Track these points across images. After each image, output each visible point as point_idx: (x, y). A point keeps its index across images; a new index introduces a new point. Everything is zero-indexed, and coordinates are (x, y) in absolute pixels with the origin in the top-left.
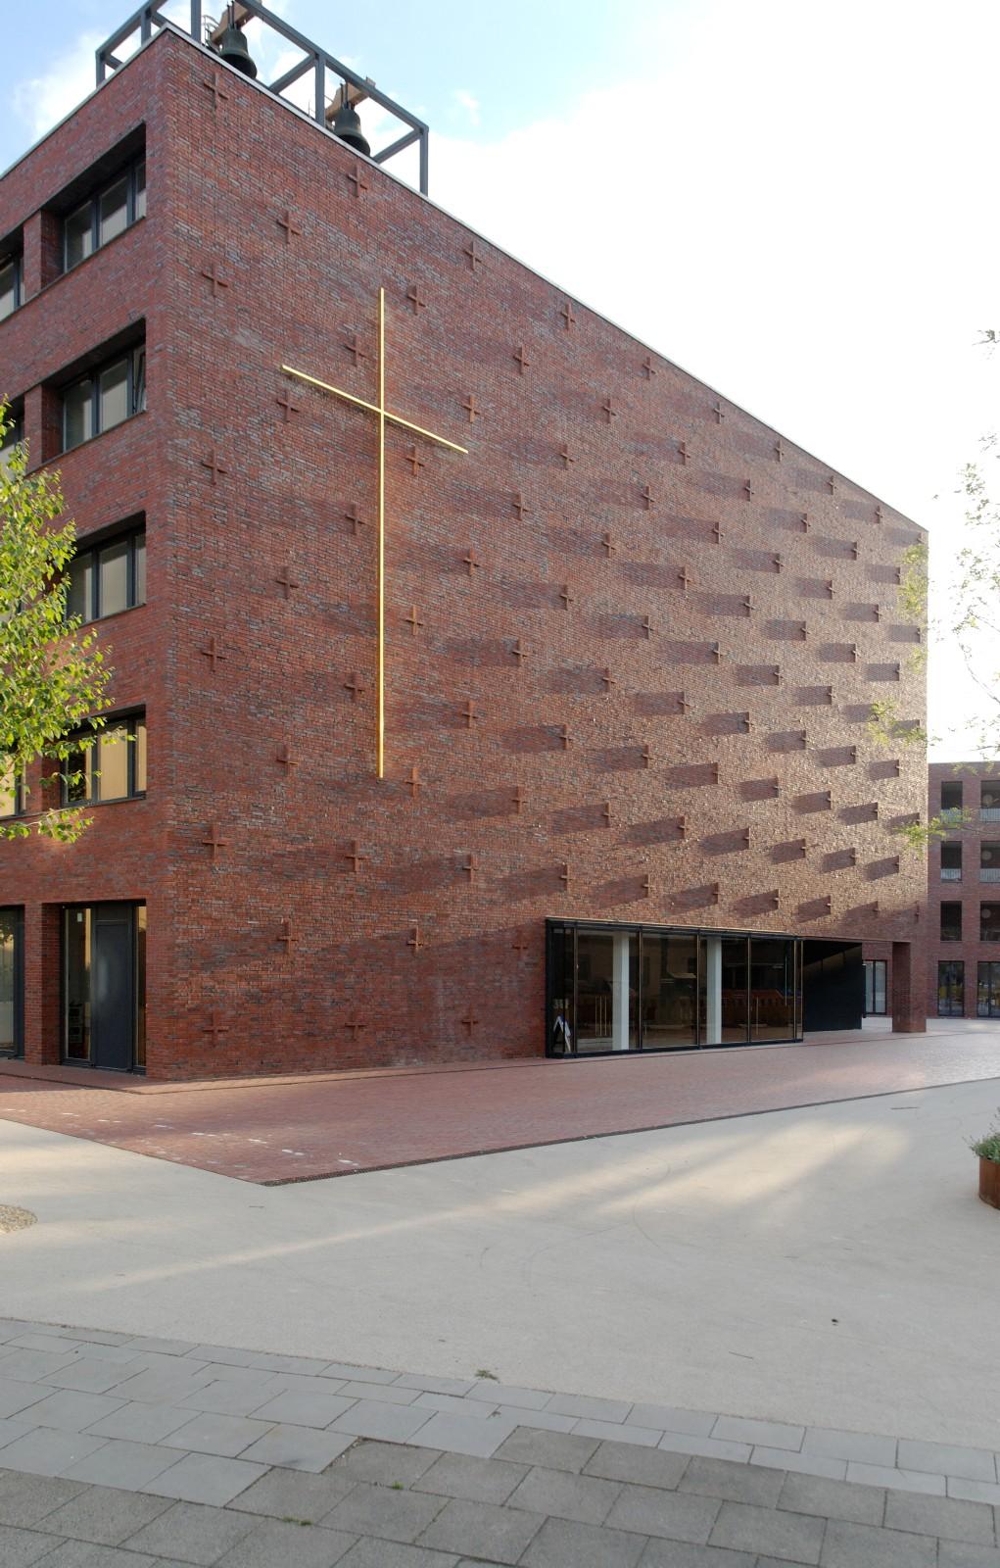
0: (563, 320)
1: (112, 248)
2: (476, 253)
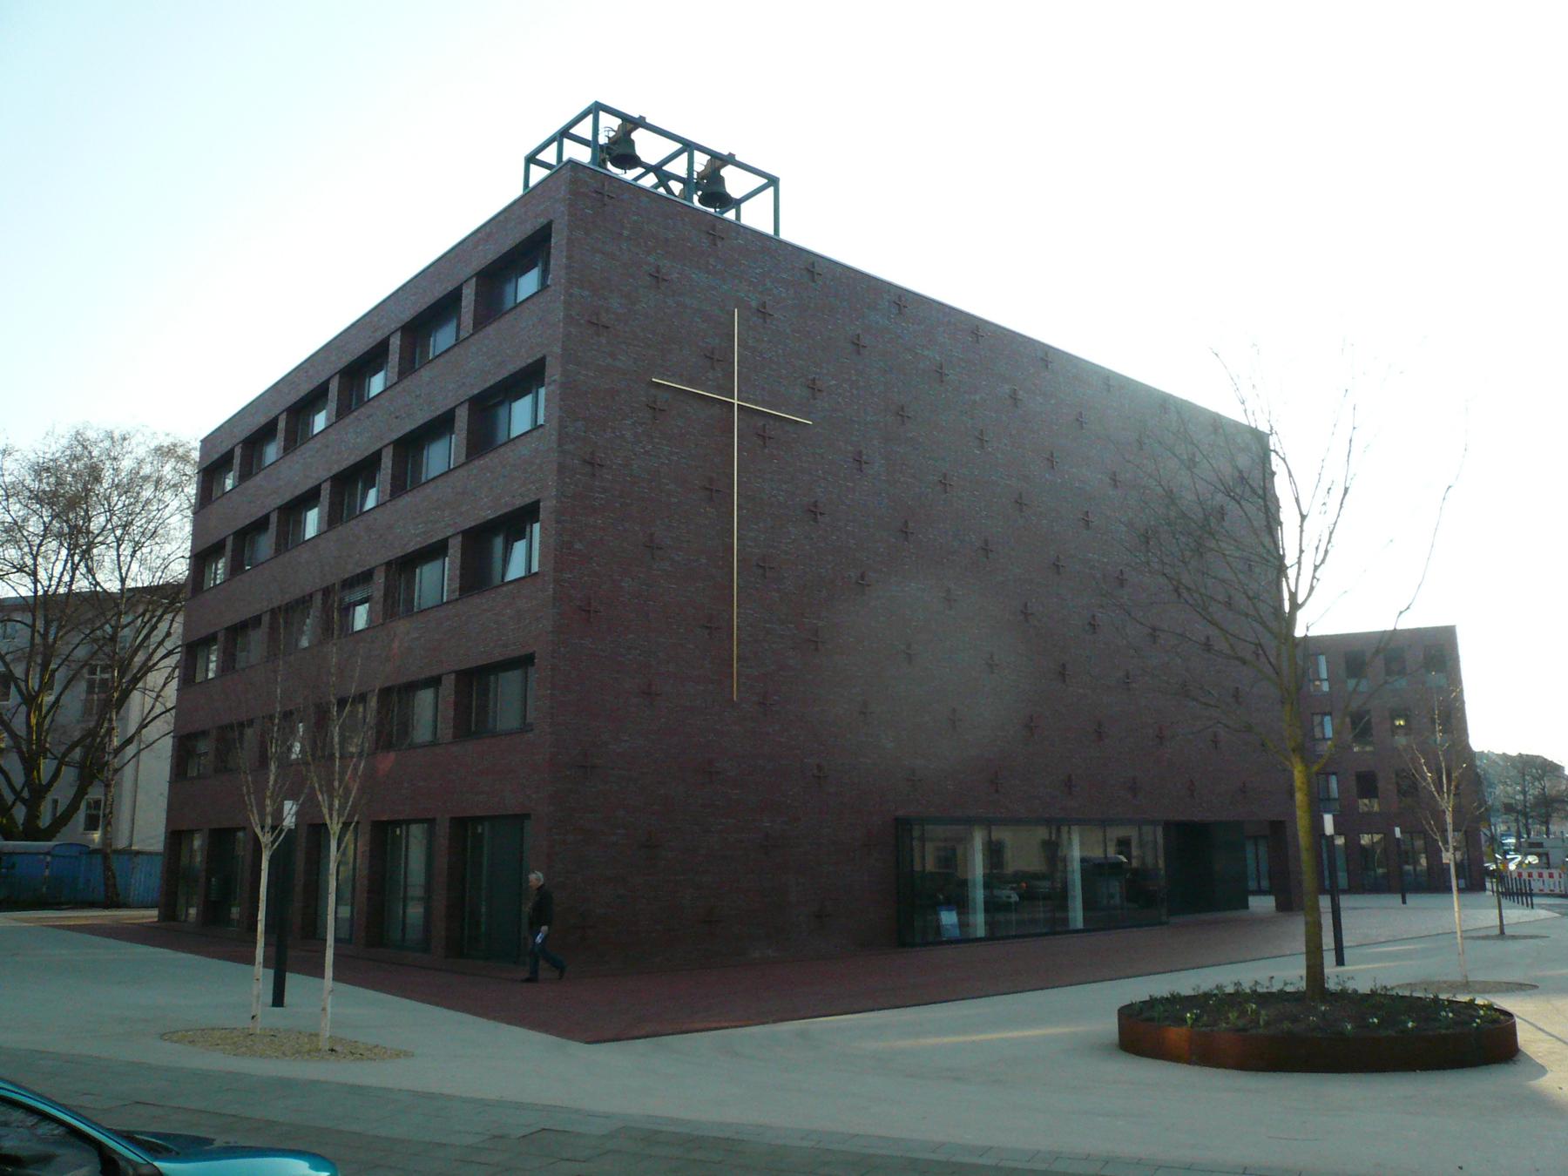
0: (897, 307)
1: (525, 305)
2: (817, 269)
